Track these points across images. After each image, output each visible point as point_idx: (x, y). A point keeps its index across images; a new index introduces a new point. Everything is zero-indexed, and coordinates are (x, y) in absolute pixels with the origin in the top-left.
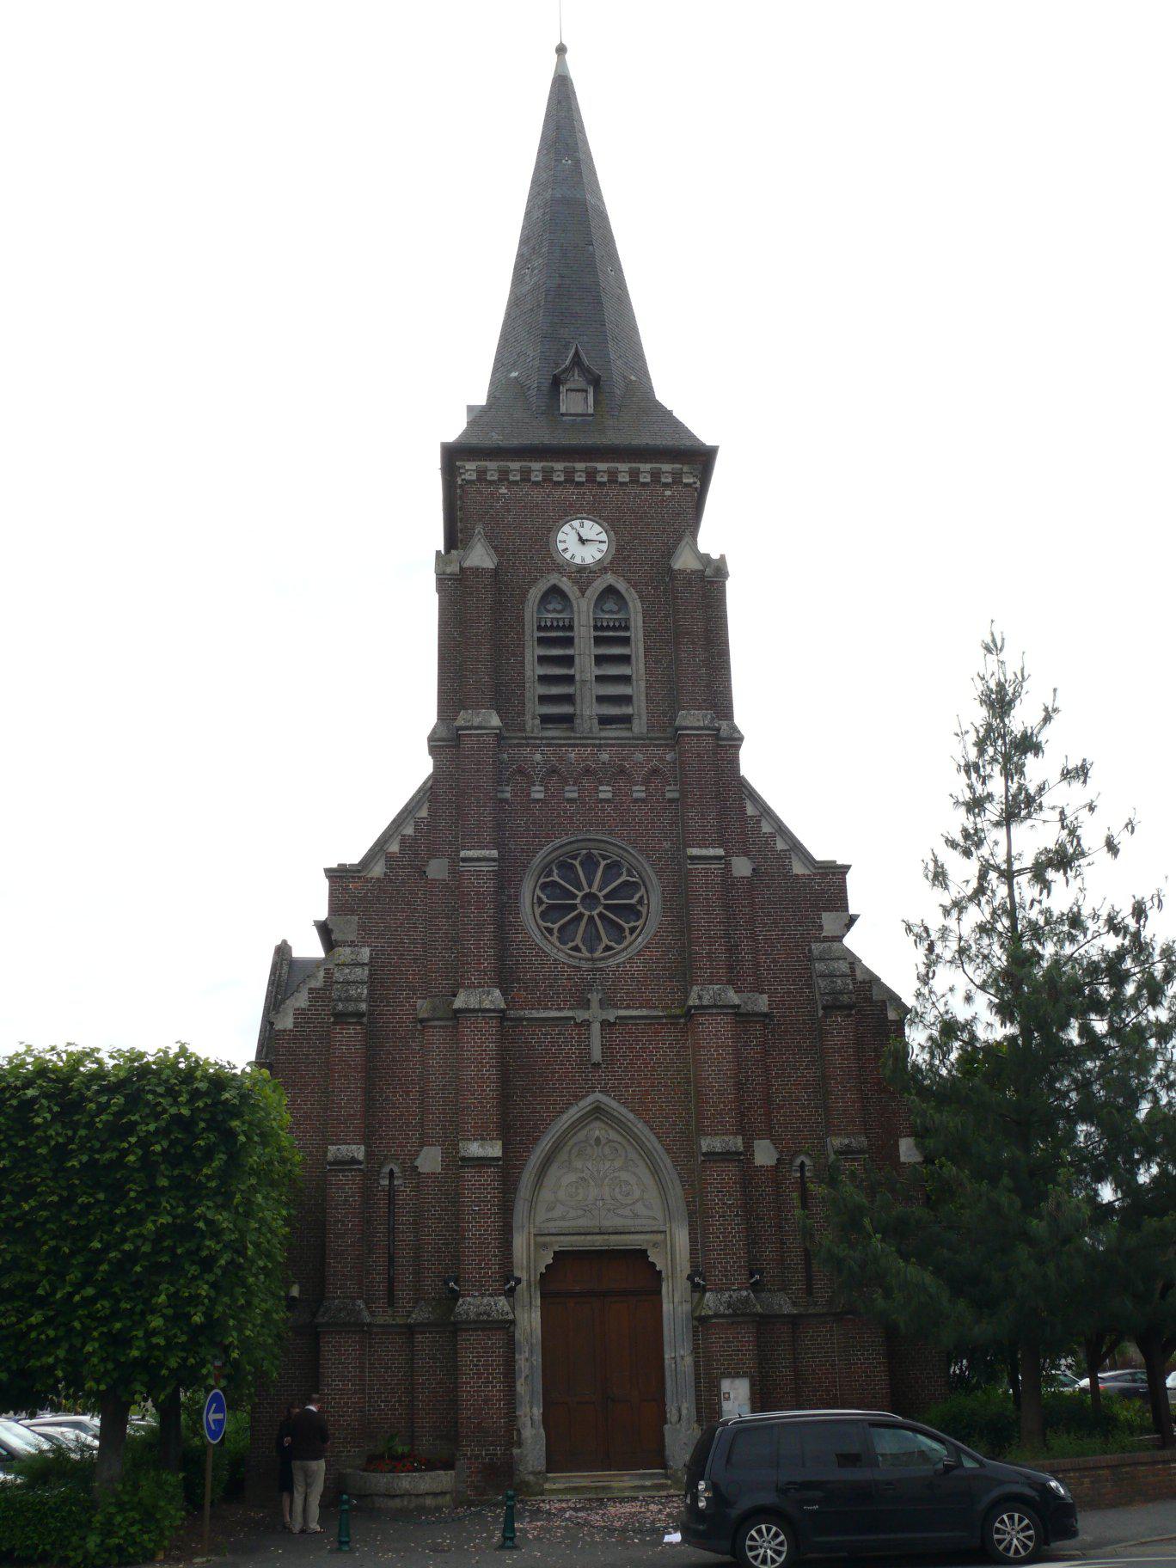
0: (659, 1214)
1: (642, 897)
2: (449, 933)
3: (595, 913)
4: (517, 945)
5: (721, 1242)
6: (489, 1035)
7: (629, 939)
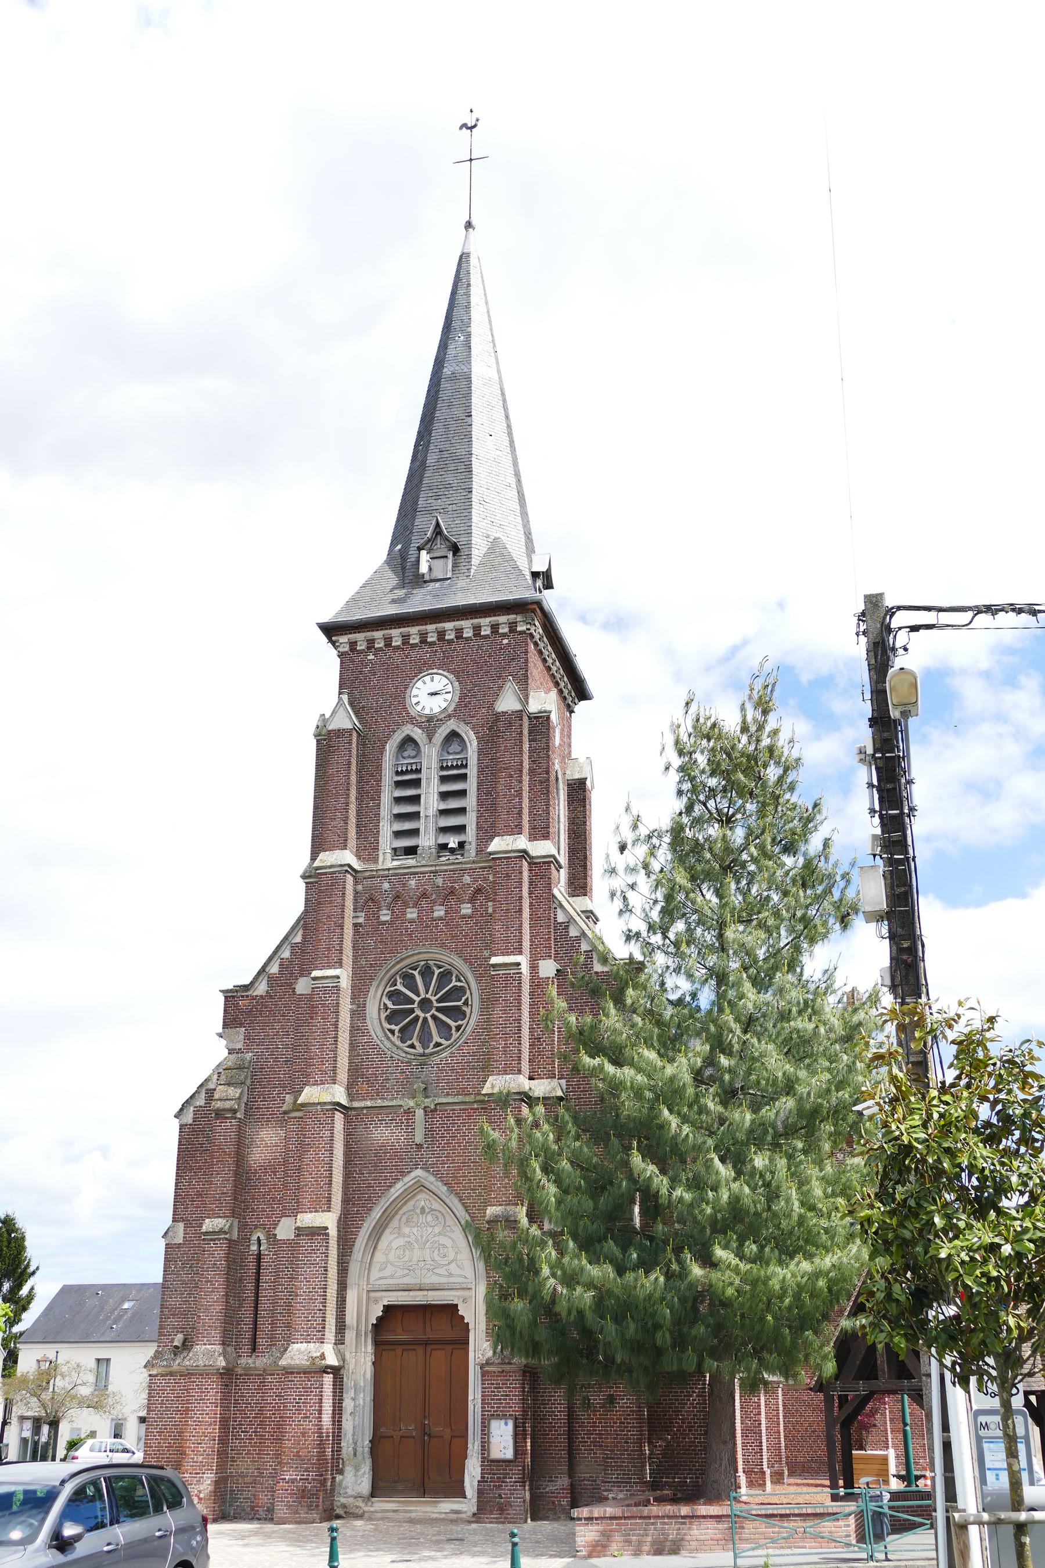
1: (467, 999)
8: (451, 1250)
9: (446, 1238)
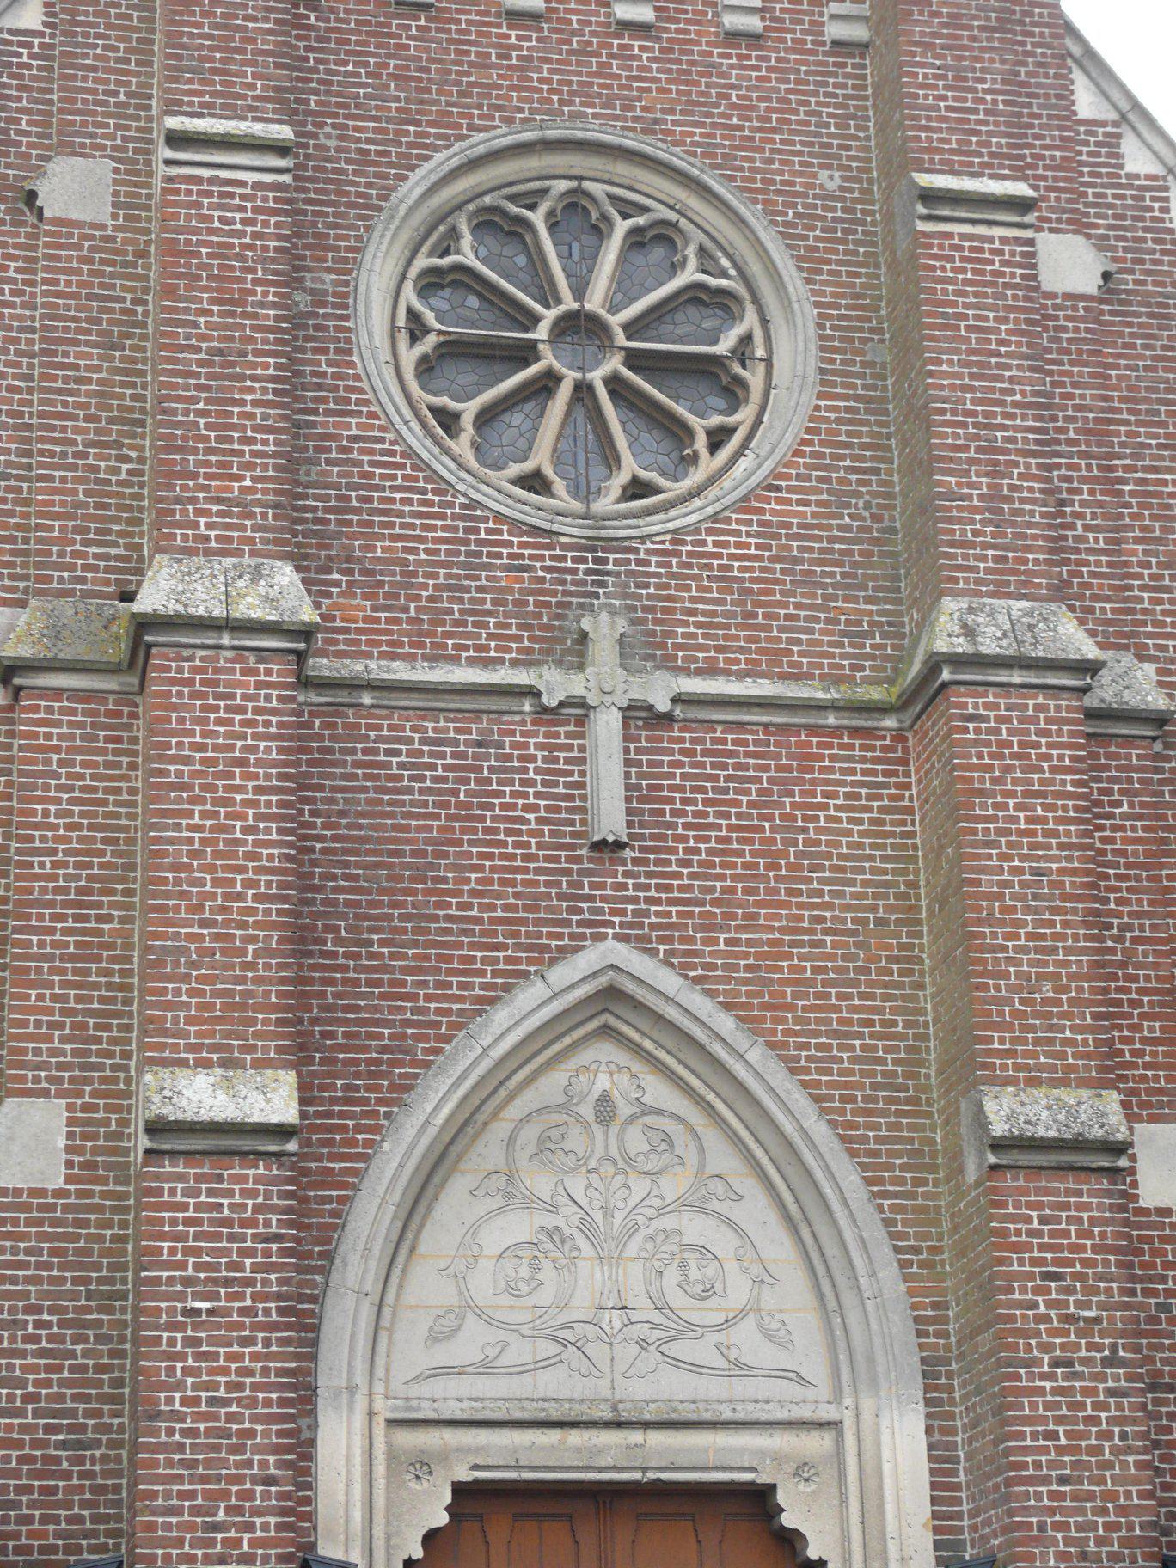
0: (815, 1368)
1: (747, 339)
2: (113, 396)
3: (597, 376)
4: (342, 450)
5: (1060, 1450)
6: (257, 711)
7: (708, 464)
8: (731, 1267)
9: (712, 1222)
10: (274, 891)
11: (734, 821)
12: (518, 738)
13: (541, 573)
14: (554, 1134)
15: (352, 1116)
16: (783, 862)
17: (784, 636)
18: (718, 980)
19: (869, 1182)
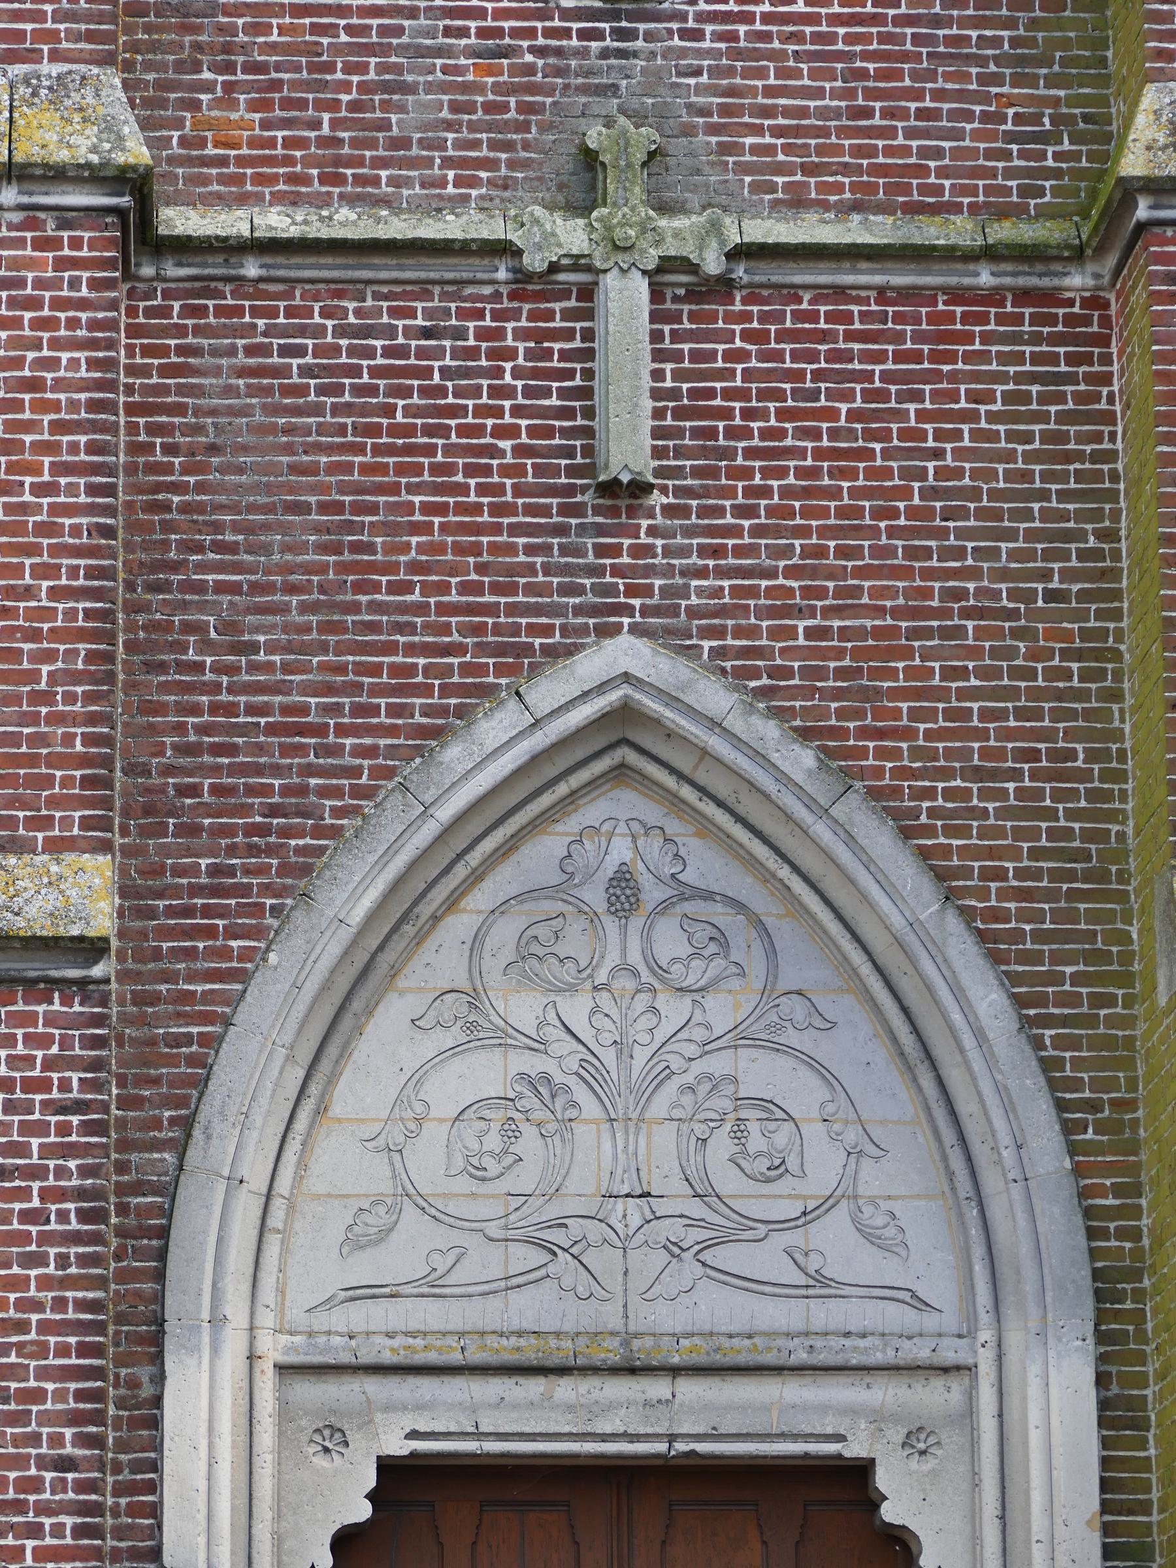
6: (59, 304)
8: (814, 1131)
10: (81, 582)
11: (825, 443)
12: (488, 322)
13: (529, 58)
14: (542, 931)
15: (223, 912)
16: (901, 505)
17: (915, 144)
18: (793, 693)
19: (1020, 1002)
